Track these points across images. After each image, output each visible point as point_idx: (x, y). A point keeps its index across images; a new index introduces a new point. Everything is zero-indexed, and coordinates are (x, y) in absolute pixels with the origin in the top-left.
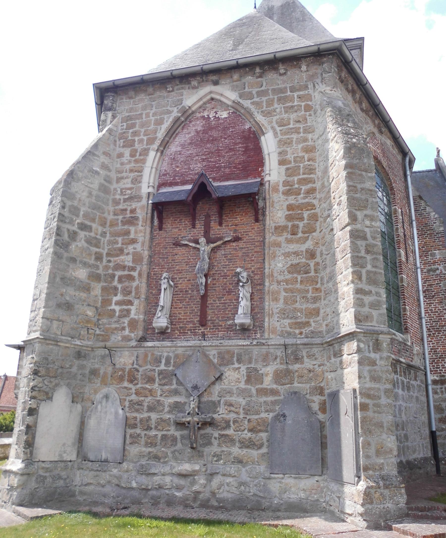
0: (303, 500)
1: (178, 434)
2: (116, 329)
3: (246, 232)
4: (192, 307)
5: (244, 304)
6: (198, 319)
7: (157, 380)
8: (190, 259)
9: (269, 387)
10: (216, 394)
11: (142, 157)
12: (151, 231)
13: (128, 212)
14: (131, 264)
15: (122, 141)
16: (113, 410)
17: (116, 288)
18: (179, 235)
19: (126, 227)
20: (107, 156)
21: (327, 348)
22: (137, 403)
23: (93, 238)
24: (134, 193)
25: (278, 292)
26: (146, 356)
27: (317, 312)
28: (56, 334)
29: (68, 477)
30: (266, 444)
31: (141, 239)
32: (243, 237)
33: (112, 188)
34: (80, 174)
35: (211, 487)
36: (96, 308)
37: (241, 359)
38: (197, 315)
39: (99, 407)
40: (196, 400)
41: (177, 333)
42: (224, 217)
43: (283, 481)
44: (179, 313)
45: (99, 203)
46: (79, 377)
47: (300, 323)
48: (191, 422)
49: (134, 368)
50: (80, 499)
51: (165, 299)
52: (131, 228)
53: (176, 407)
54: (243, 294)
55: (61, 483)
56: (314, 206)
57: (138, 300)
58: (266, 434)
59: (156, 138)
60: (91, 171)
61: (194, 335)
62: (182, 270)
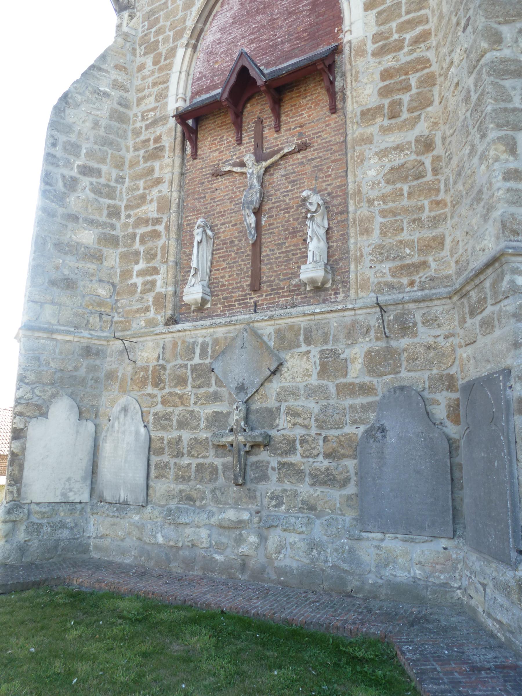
0: (418, 582)
1: (219, 462)
2: (138, 311)
3: (317, 133)
4: (240, 265)
5: (316, 246)
6: (249, 282)
7: (190, 380)
8: (235, 192)
9: (357, 381)
10: (274, 398)
11: (168, 62)
12: (183, 164)
13: (151, 142)
14: (155, 215)
15: (143, 47)
16: (133, 428)
17: (137, 253)
18: (220, 160)
19: (149, 164)
20: (121, 71)
21: (458, 303)
22: (164, 416)
23: (104, 185)
24: (158, 114)
25: (370, 219)
26: (175, 345)
27: (440, 241)
28: (50, 324)
29: (76, 525)
30: (354, 479)
31: (167, 177)
32: (313, 142)
33: (131, 114)
34: (79, 98)
35: (266, 549)
36: (114, 285)
37: (311, 336)
38: (248, 276)
39: (116, 424)
40: (242, 407)
41: (219, 308)
42: (283, 118)
43: (383, 545)
44: (223, 277)
45: (111, 136)
46: (90, 383)
47: (409, 266)
48: (234, 444)
49: (159, 365)
50: (95, 556)
51: (200, 257)
52: (154, 164)
53: (216, 421)
54: (313, 230)
55: (65, 533)
56: (428, 60)
57: (165, 266)
58: (355, 461)
59: (185, 28)
60: (97, 92)
61: (243, 308)
62: (225, 211)
